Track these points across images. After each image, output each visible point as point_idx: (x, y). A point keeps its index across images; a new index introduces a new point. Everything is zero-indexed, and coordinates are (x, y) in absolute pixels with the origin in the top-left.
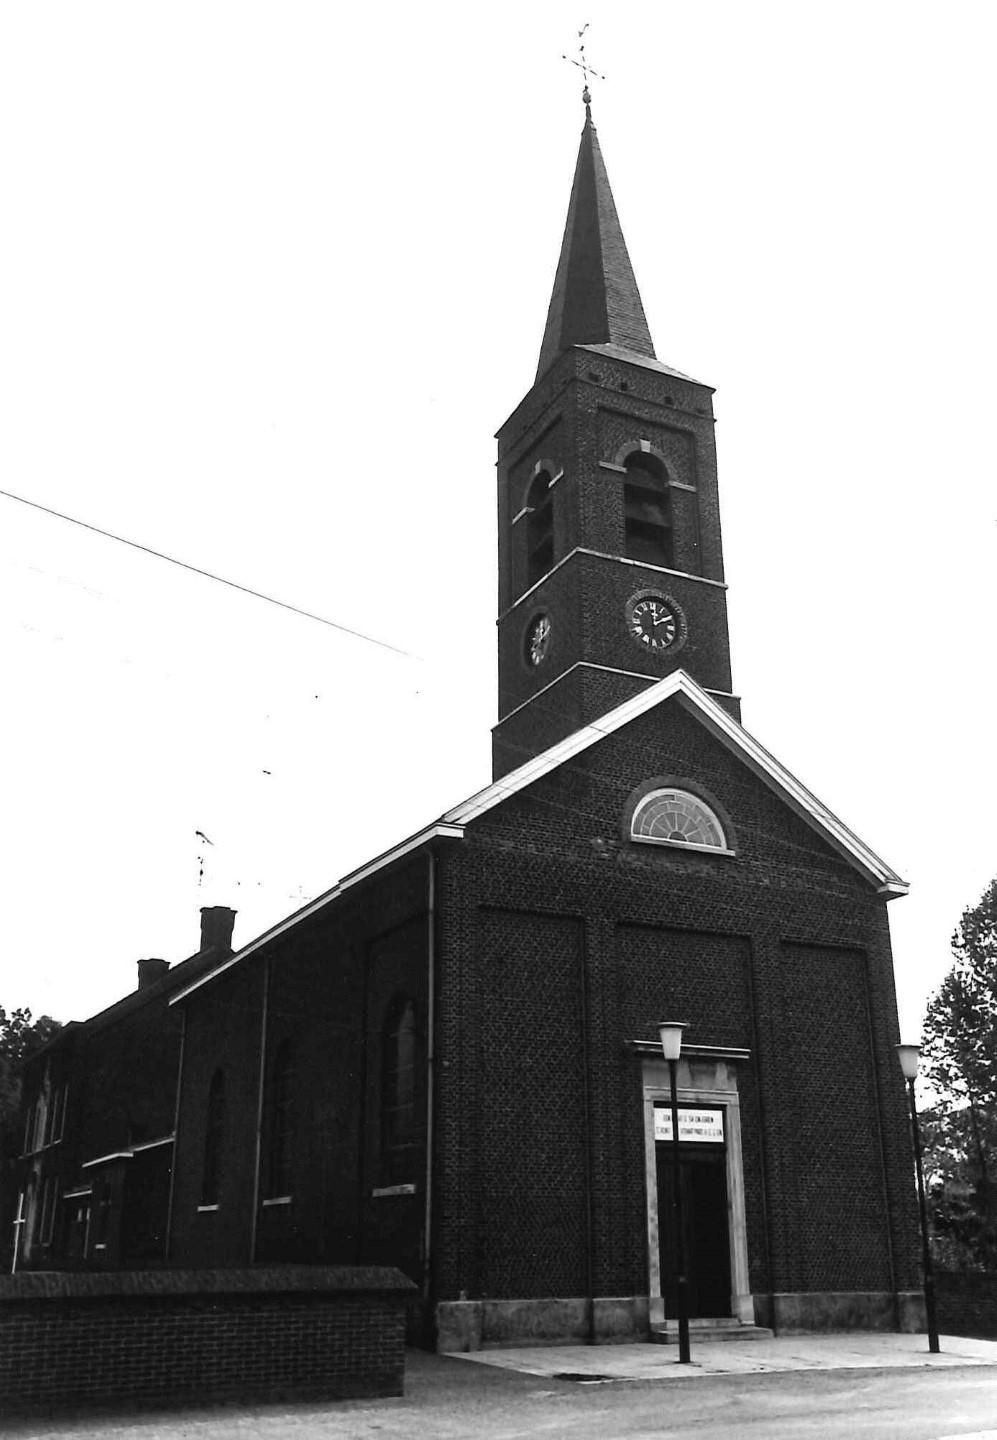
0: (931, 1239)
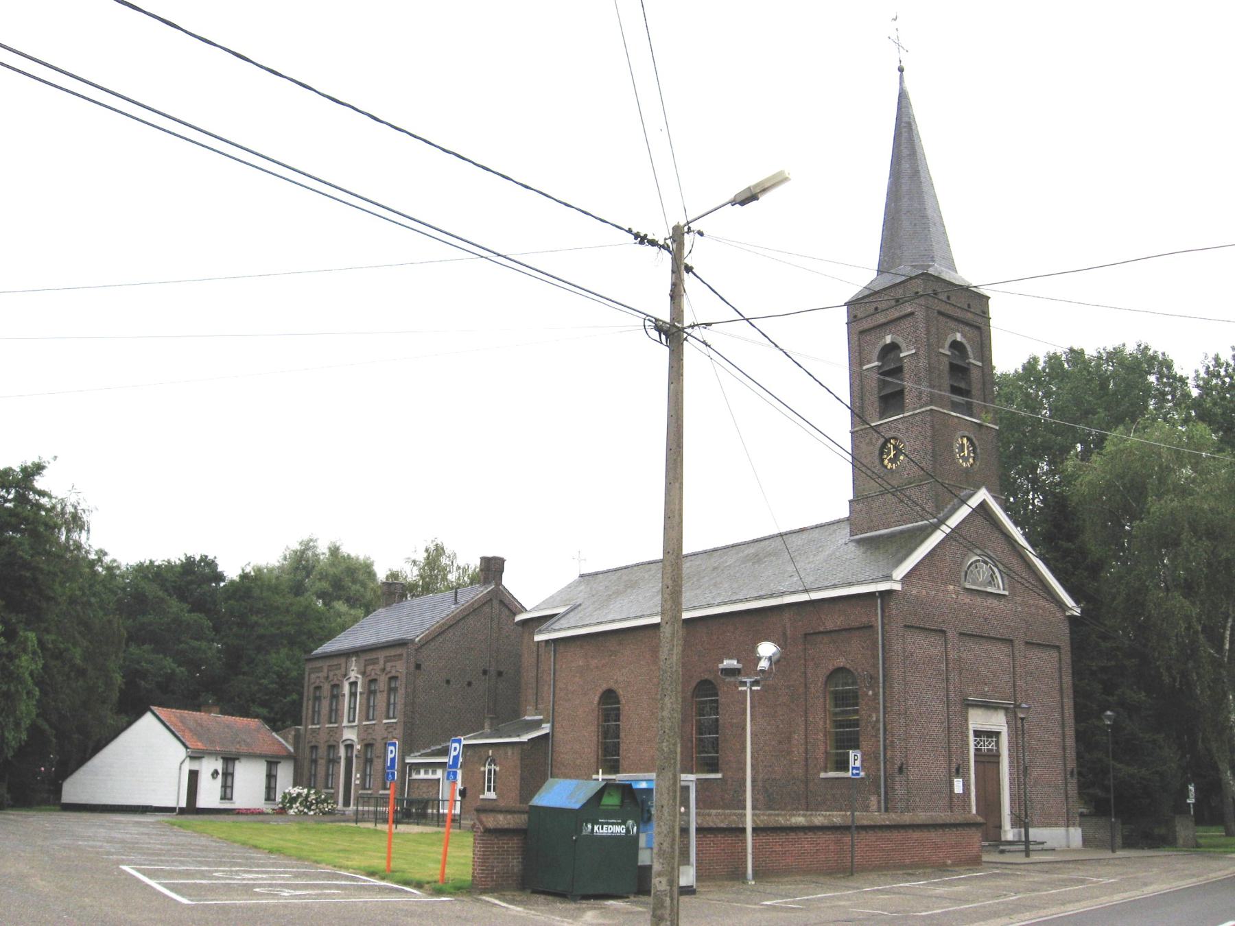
0: (46, 859)
